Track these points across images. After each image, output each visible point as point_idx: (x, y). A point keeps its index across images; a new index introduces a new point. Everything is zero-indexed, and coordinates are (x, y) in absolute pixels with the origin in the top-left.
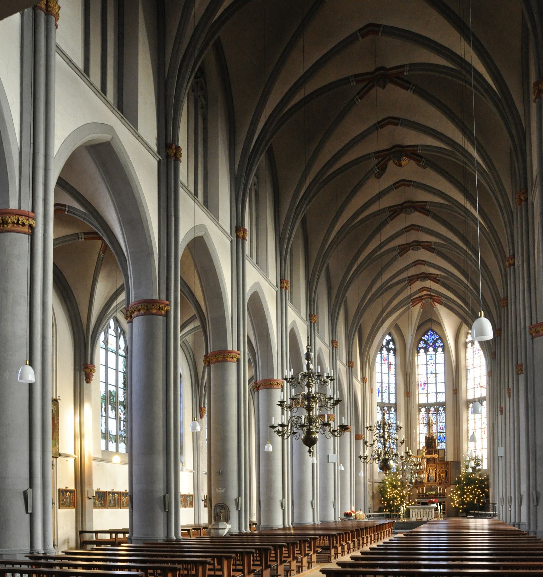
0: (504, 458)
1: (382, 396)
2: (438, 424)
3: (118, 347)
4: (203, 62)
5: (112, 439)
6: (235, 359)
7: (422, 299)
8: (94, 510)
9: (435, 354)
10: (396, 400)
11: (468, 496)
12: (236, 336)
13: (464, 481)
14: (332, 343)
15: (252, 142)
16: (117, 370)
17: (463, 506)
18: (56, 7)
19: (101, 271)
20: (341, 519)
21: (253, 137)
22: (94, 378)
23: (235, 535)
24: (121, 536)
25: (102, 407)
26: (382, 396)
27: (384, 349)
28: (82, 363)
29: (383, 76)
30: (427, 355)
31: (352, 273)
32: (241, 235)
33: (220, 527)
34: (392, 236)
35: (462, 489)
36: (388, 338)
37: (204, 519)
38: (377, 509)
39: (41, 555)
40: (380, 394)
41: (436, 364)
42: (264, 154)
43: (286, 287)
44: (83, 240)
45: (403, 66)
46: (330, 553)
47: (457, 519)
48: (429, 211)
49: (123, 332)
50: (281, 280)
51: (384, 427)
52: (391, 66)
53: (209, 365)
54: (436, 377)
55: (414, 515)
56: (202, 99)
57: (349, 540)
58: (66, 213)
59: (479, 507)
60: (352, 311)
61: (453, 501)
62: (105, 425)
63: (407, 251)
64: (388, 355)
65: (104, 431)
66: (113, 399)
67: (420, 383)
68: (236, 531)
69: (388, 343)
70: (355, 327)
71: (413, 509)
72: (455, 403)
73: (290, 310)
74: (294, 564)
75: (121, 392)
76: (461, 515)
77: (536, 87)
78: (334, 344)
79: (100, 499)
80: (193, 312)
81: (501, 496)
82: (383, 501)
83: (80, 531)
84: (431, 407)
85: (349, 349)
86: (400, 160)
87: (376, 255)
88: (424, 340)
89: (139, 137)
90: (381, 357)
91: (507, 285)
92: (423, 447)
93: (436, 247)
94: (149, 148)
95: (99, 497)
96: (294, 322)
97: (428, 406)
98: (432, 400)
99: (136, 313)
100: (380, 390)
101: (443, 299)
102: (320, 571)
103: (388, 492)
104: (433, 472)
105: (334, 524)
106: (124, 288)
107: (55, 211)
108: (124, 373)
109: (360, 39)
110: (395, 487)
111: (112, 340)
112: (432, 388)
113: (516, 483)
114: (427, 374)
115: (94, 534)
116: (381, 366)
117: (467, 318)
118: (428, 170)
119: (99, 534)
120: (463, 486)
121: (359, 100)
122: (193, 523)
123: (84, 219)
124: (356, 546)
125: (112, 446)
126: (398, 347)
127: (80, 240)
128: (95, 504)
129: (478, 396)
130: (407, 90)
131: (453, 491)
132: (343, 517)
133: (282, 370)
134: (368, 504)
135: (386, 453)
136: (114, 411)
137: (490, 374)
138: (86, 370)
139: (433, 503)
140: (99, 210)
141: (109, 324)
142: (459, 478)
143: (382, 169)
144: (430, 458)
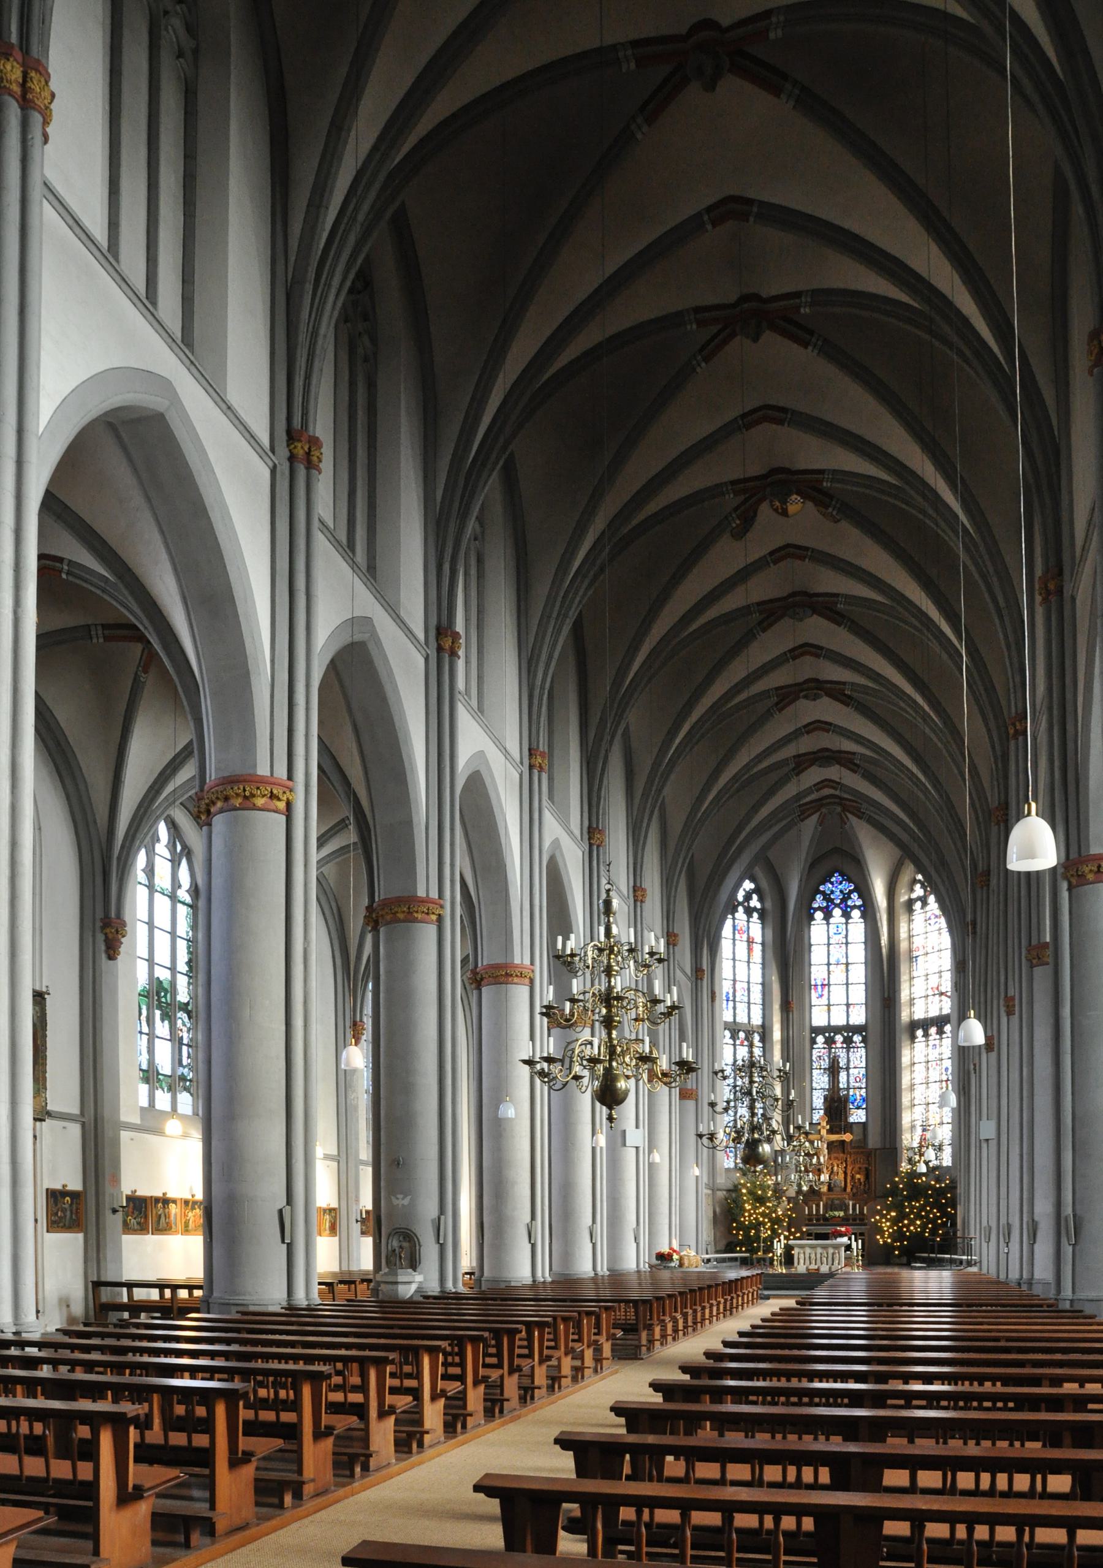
0: (993, 1144)
1: (734, 1008)
2: (851, 1071)
3: (176, 884)
4: (367, 259)
5: (164, 1084)
6: (434, 917)
7: (822, 805)
8: (125, 1238)
9: (847, 923)
10: (764, 1017)
11: (912, 1222)
12: (435, 870)
13: (903, 1190)
14: (635, 891)
15: (473, 441)
16: (173, 934)
17: (902, 1243)
18: (46, 94)
19: (140, 712)
20: (651, 1266)
21: (476, 431)
22: (123, 949)
23: (435, 1298)
24: (183, 1294)
25: (140, 1014)
26: (734, 1008)
27: (740, 909)
28: (100, 914)
29: (755, 315)
30: (828, 924)
31: (677, 741)
32: (447, 643)
33: (400, 1279)
34: (764, 665)
35: (899, 1207)
36: (748, 885)
37: (365, 1261)
38: (722, 1245)
39: (9, 1336)
40: (731, 1004)
41: (847, 943)
42: (495, 474)
43: (540, 767)
44: (101, 640)
45: (798, 295)
46: (639, 1340)
47: (889, 1270)
48: (842, 616)
49: (188, 852)
50: (530, 750)
51: (751, 1073)
52: (774, 292)
53: (375, 930)
54: (847, 971)
55: (802, 1261)
56: (366, 339)
57: (676, 1311)
58: (64, 576)
59: (936, 1244)
60: (676, 825)
61: (881, 1232)
62: (149, 1052)
63: (794, 701)
64: (748, 921)
65: (144, 1067)
66: (165, 996)
67: (813, 983)
68: (433, 1288)
69: (748, 897)
70: (681, 861)
71: (802, 1247)
72: (886, 1029)
73: (549, 818)
74: (567, 1364)
75: (182, 982)
76: (897, 1261)
77: (1095, 342)
78: (639, 893)
79: (136, 1213)
80: (346, 811)
81: (984, 1223)
82: (735, 1228)
83: (93, 1282)
84: (836, 1034)
85: (668, 905)
86: (785, 502)
87: (729, 706)
88: (823, 893)
89: (228, 409)
90: (734, 926)
91: (1006, 777)
92: (822, 1118)
93: (855, 695)
94: (251, 437)
95: (134, 1208)
96: (556, 843)
97: (829, 1032)
98: (838, 1020)
99: (219, 804)
100: (731, 995)
101: (865, 805)
102: (651, 1385)
103: (745, 1210)
104: (839, 1170)
105: (635, 1277)
106: (192, 752)
107: (41, 571)
108: (188, 941)
109: (709, 227)
110: (761, 1200)
111: (163, 869)
112: (838, 995)
113: (1025, 1196)
114: (829, 964)
115: (125, 1290)
116: (734, 944)
117: (915, 848)
118: (845, 525)
119: (135, 1290)
120: (902, 1202)
121: (703, 364)
122: (336, 1269)
123: (103, 591)
124: (690, 1324)
125: (163, 1100)
126: (769, 905)
127: (95, 640)
128: (125, 1224)
129: (934, 1013)
130: (806, 348)
131: (881, 1210)
132: (654, 1261)
133: (526, 947)
134: (705, 1233)
135: (754, 1128)
136: (166, 1022)
137: (960, 966)
138: (108, 930)
139: (842, 1235)
140: (138, 571)
141: (157, 830)
142: (895, 1185)
143: (748, 519)
144: (833, 1142)
